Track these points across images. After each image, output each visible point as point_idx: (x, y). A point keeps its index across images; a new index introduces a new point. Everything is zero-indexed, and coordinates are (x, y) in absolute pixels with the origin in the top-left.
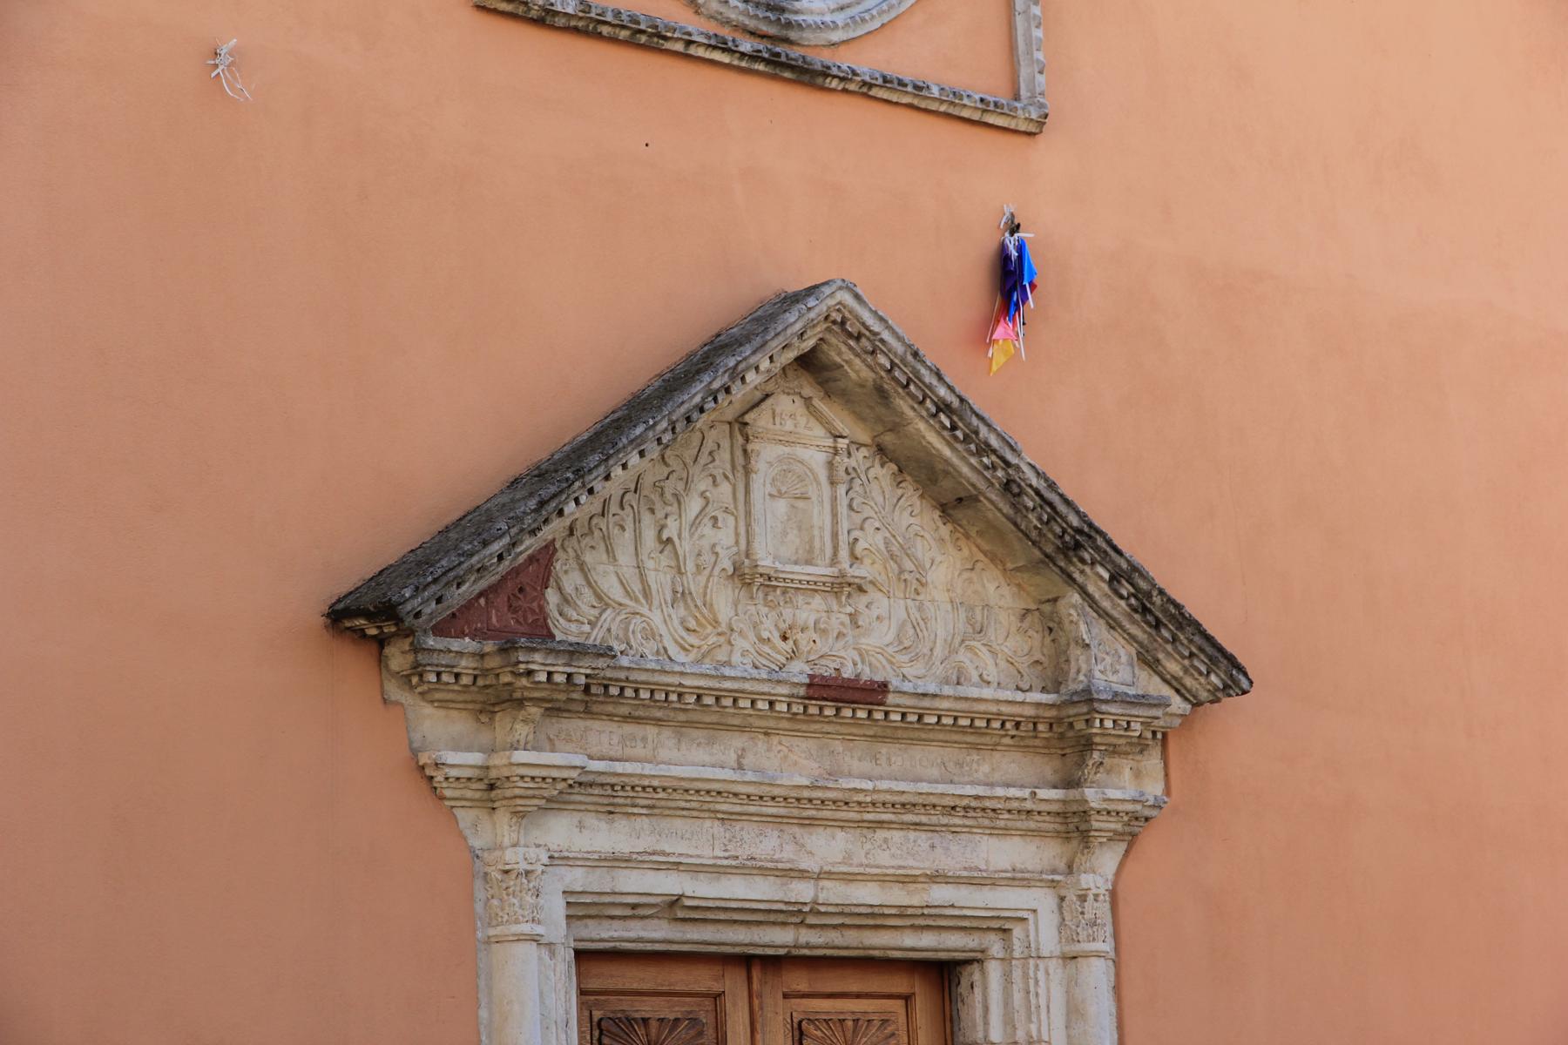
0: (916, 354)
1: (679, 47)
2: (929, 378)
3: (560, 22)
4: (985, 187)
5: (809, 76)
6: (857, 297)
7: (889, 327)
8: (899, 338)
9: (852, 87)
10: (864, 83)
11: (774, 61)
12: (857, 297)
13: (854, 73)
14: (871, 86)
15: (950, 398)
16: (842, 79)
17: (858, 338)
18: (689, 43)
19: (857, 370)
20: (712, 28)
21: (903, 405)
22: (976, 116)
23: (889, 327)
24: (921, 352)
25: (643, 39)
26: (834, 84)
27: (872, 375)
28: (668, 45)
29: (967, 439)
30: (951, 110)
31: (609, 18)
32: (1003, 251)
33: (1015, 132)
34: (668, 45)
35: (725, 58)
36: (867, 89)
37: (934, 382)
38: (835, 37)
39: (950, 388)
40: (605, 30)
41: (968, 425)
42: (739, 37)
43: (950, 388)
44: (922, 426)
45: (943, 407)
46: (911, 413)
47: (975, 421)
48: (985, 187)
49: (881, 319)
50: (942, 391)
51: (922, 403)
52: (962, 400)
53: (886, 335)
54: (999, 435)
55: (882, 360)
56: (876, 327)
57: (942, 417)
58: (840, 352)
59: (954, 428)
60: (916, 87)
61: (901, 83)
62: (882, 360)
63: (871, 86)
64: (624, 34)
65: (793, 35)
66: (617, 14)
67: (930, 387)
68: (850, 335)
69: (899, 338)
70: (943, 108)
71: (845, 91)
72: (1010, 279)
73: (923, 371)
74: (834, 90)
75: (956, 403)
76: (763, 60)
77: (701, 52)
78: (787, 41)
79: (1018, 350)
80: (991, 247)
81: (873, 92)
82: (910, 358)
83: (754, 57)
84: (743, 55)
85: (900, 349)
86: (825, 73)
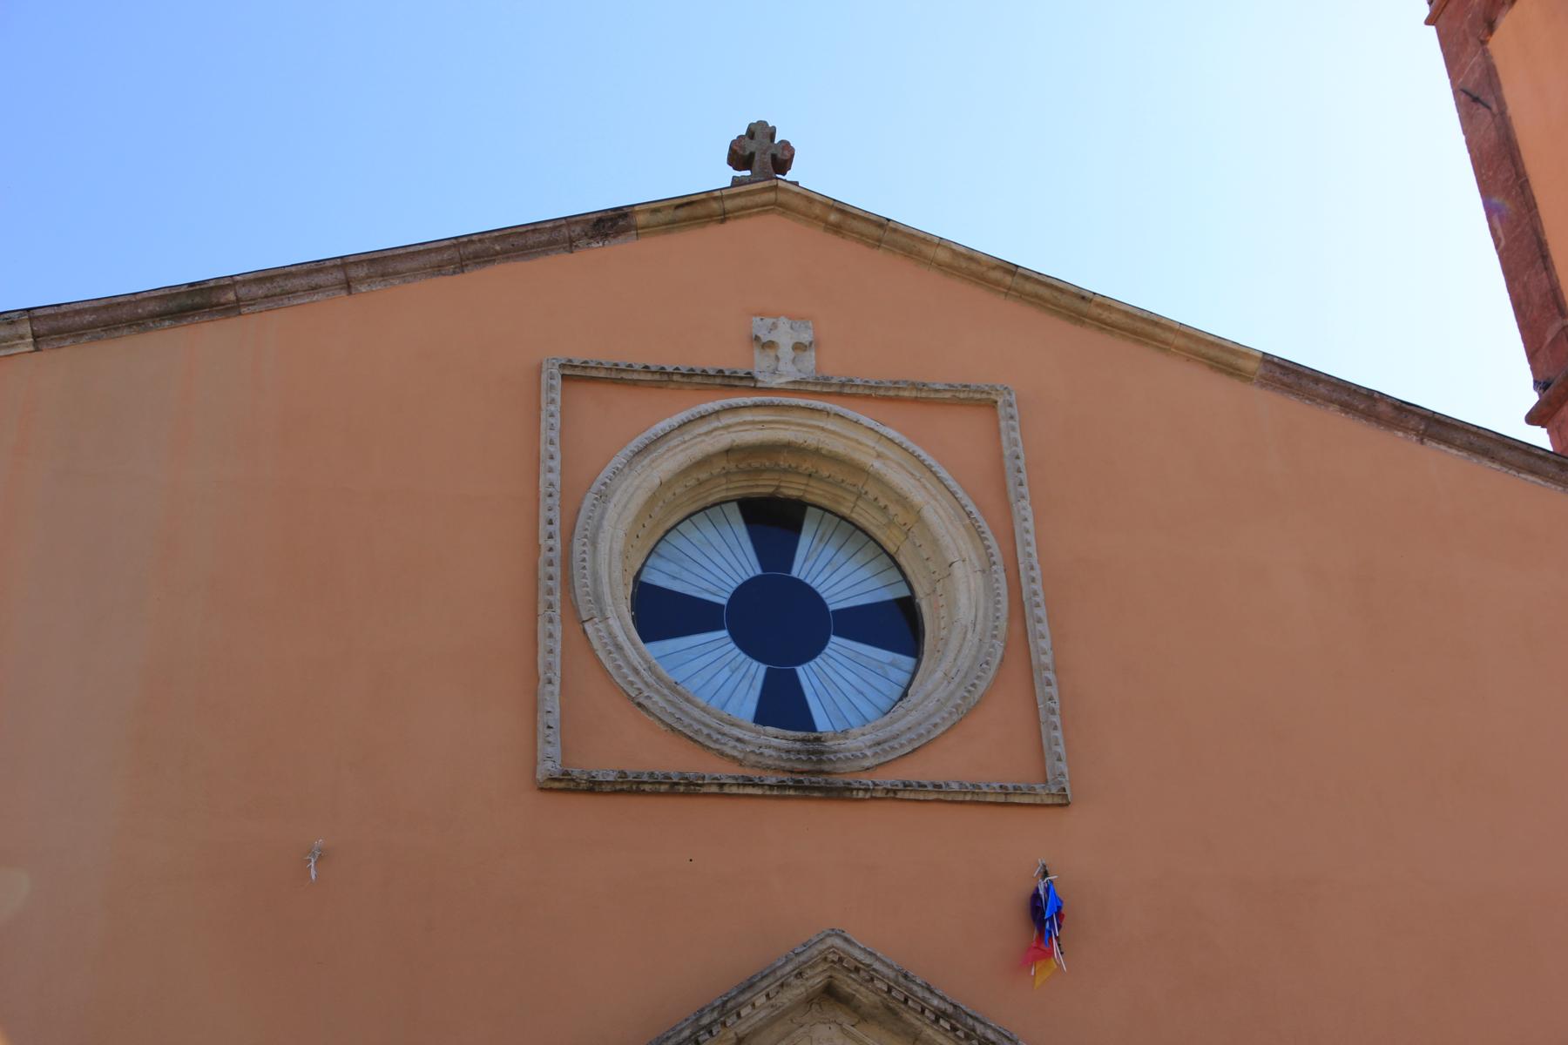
0: (906, 976)
1: (714, 789)
2: (920, 993)
3: (608, 788)
4: (1017, 851)
5: (839, 793)
6: (846, 940)
7: (878, 959)
8: (889, 966)
9: (879, 795)
10: (888, 791)
11: (798, 786)
12: (846, 940)
13: (875, 784)
14: (895, 792)
15: (943, 1006)
16: (866, 790)
17: (857, 970)
18: (722, 785)
19: (865, 996)
20: (739, 771)
21: (910, 1017)
22: (1002, 799)
23: (878, 959)
24: (911, 974)
25: (682, 789)
26: (861, 794)
27: (877, 999)
28: (704, 790)
29: (968, 1037)
30: (976, 798)
31: (645, 778)
32: (1036, 896)
33: (696, 741)
34: (704, 790)
35: (759, 791)
36: (891, 794)
37: (927, 995)
38: (867, 763)
39: (942, 998)
40: (647, 787)
41: (965, 1025)
42: (763, 774)
43: (942, 998)
44: (929, 1031)
45: (940, 1015)
46: (919, 1023)
47: (970, 1022)
48: (1017, 851)
49: (871, 954)
50: (935, 1002)
51: (923, 1011)
52: (955, 1007)
53: (877, 965)
54: (994, 1030)
55: (879, 984)
56: (868, 960)
57: (942, 1022)
58: (848, 984)
59: (954, 1029)
60: (935, 786)
61: (921, 785)
62: (879, 984)
63: (895, 792)
64: (663, 788)
65: (826, 767)
66: (651, 775)
67: (924, 1000)
68: (848, 970)
69: (889, 966)
70: (968, 798)
71: (873, 798)
72: (1042, 914)
73: (915, 988)
74: (862, 800)
75: (950, 1009)
76: (790, 787)
77: (734, 790)
78: (822, 772)
79: (1060, 966)
80: (1030, 891)
81: (900, 795)
82: (901, 979)
83: (781, 786)
84: (771, 787)
85: (891, 974)
86: (848, 788)
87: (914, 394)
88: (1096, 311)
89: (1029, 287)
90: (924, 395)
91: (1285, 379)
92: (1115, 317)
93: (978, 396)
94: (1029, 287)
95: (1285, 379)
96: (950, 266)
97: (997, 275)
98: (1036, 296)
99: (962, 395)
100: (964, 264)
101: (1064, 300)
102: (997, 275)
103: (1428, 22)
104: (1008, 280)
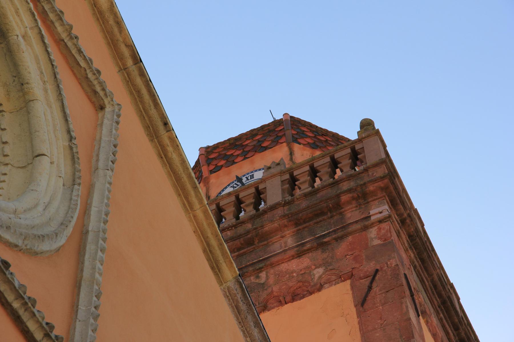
30: (21, 312)
70: (16, 305)
87: (64, 36)
88: (166, 141)
89: (139, 81)
90: (69, 44)
91: (241, 304)
92: (174, 156)
93: (98, 89)
94: (139, 81)
95: (241, 304)
96: (101, 13)
97: (126, 52)
98: (139, 92)
99: (90, 75)
100: (111, 22)
101: (153, 112)
102: (126, 52)
103: (378, 129)
104: (130, 62)
